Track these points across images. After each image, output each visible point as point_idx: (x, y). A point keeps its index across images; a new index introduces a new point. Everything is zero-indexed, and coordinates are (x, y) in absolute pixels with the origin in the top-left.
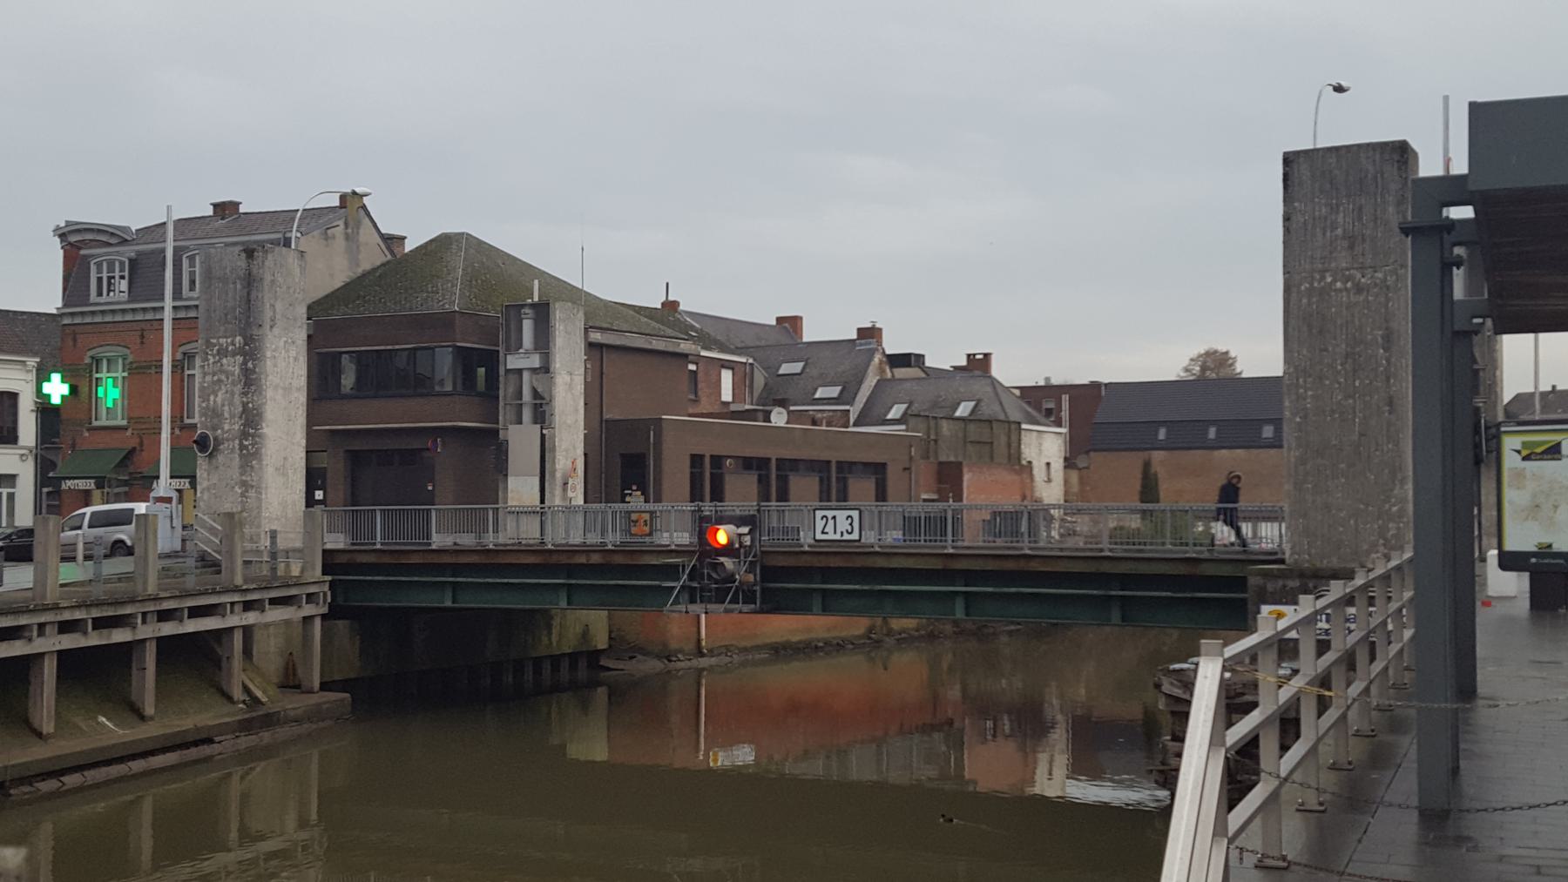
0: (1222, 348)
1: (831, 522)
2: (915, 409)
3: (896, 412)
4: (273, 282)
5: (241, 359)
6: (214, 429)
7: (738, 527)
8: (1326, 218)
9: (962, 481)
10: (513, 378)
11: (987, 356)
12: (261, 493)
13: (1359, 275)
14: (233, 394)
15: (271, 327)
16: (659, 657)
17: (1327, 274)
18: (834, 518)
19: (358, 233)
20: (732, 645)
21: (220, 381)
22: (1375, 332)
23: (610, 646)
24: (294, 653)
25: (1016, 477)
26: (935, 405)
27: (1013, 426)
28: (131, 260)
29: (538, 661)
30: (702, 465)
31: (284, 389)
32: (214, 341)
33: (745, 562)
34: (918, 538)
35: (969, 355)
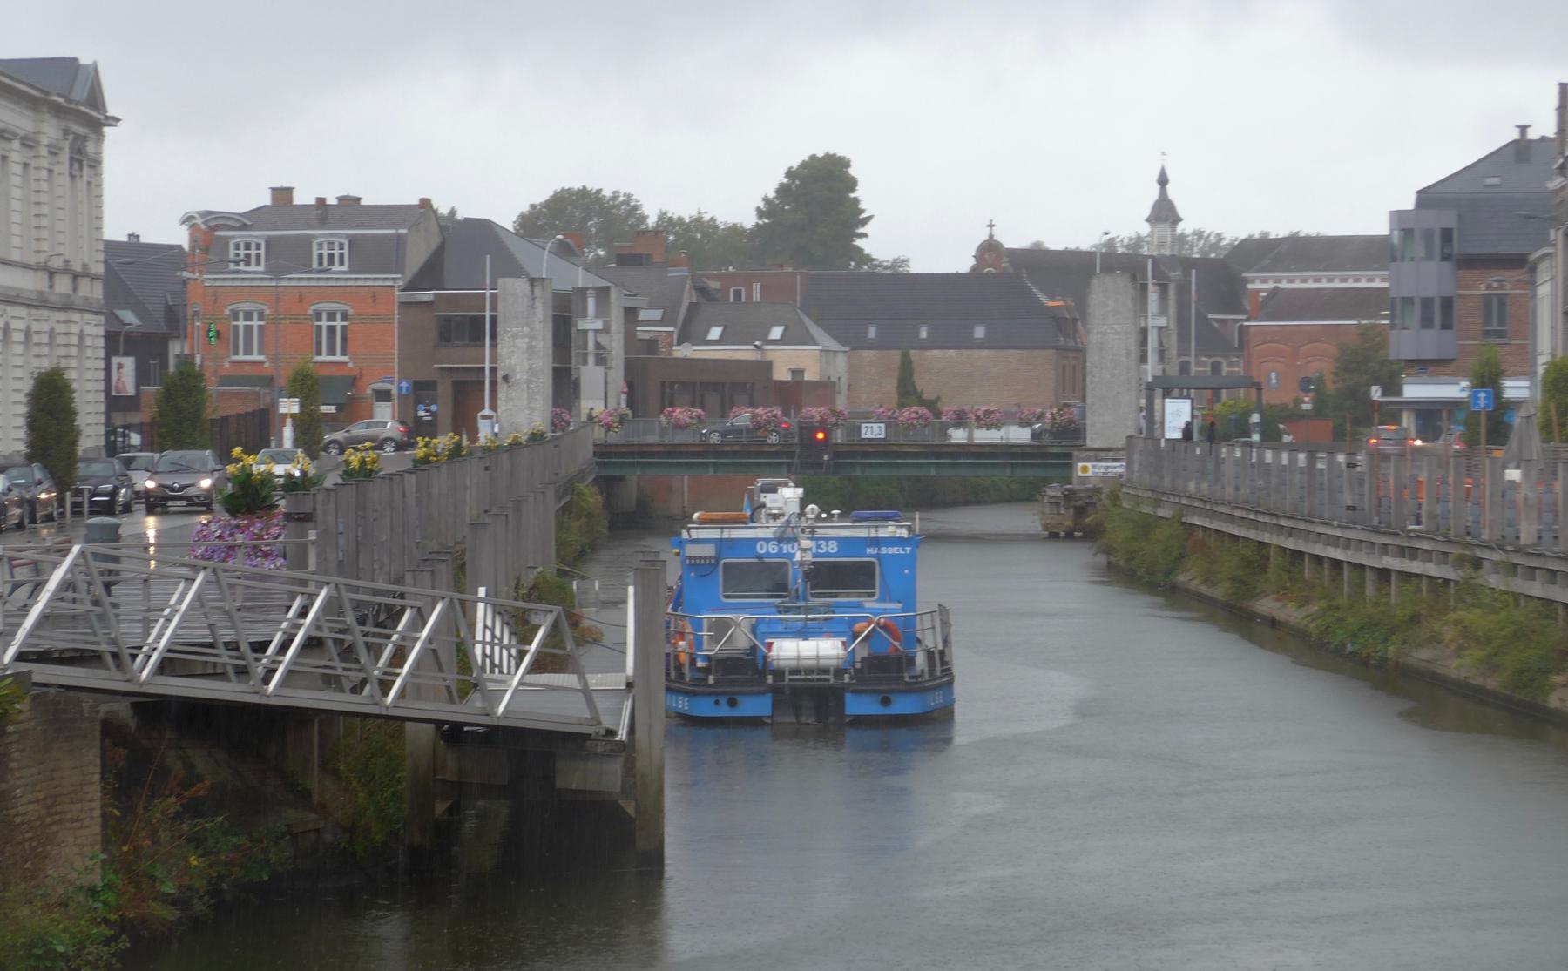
1: (870, 430)
32: (509, 329)
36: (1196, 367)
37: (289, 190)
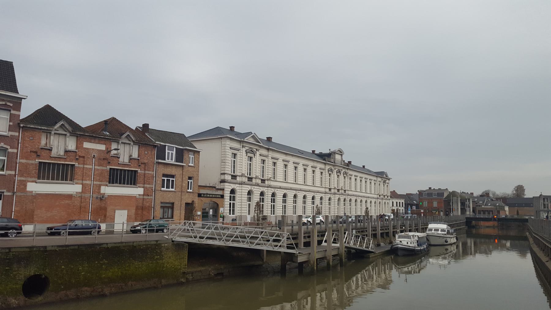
0: (521, 185)
3: (489, 204)
36: (169, 188)
37: (473, 193)
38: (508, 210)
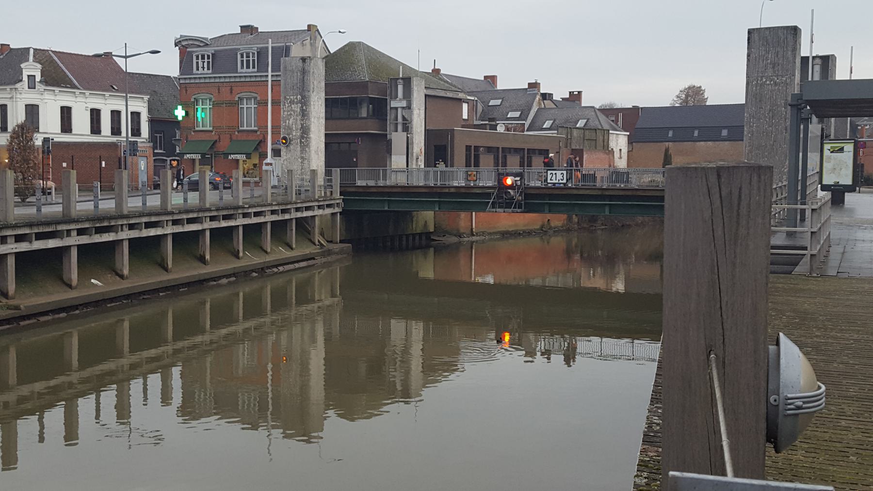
1: (554, 176)
2: (557, 122)
3: (547, 124)
4: (313, 72)
5: (300, 105)
6: (288, 135)
7: (515, 177)
8: (764, 56)
9: (583, 158)
10: (394, 111)
11: (580, 93)
12: (310, 162)
13: (776, 79)
14: (297, 120)
15: (313, 92)
16: (455, 236)
17: (764, 78)
18: (556, 174)
19: (315, 43)
20: (485, 231)
21: (291, 114)
22: (782, 101)
23: (435, 230)
24: (324, 228)
25: (608, 156)
26: (567, 121)
27: (605, 132)
28: (212, 54)
29: (407, 236)
30: (470, 151)
31: (317, 118)
33: (518, 192)
34: (578, 184)
35: (570, 92)
38: (625, 151)
